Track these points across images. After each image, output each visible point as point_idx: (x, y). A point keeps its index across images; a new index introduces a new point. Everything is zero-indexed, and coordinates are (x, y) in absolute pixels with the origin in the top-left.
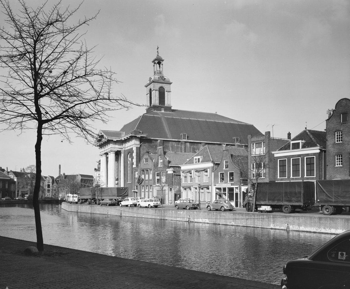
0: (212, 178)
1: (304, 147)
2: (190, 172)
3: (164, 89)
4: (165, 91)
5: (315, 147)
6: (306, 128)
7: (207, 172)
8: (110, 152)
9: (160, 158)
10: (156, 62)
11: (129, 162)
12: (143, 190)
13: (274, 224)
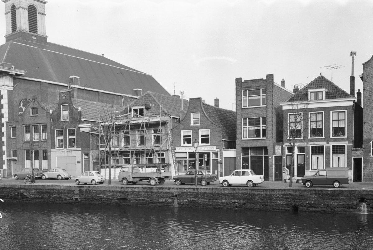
3: (35, 8)
4: (37, 13)
5: (336, 98)
6: (321, 73)
9: (64, 108)
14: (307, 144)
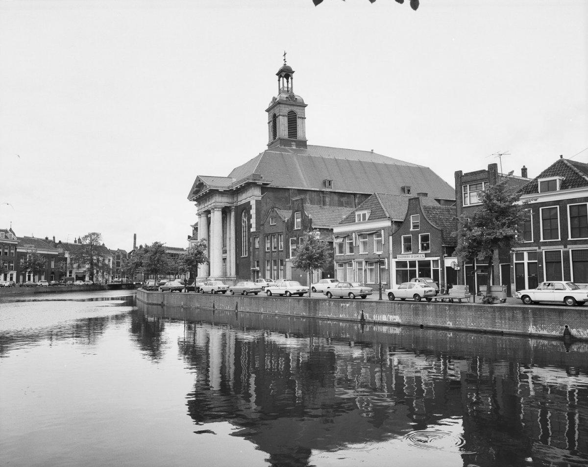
0: (389, 245)
1: (564, 186)
2: (347, 236)
6: (561, 156)
7: (380, 236)
8: (213, 209)
10: (283, 74)
11: (243, 224)
12: (269, 268)
13: (535, 325)
14: (539, 248)
